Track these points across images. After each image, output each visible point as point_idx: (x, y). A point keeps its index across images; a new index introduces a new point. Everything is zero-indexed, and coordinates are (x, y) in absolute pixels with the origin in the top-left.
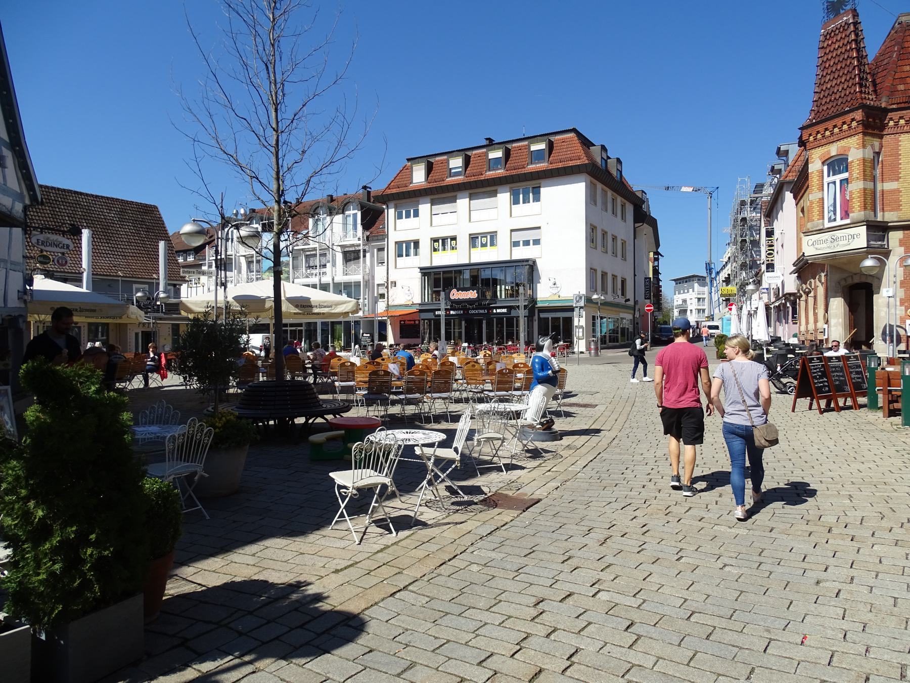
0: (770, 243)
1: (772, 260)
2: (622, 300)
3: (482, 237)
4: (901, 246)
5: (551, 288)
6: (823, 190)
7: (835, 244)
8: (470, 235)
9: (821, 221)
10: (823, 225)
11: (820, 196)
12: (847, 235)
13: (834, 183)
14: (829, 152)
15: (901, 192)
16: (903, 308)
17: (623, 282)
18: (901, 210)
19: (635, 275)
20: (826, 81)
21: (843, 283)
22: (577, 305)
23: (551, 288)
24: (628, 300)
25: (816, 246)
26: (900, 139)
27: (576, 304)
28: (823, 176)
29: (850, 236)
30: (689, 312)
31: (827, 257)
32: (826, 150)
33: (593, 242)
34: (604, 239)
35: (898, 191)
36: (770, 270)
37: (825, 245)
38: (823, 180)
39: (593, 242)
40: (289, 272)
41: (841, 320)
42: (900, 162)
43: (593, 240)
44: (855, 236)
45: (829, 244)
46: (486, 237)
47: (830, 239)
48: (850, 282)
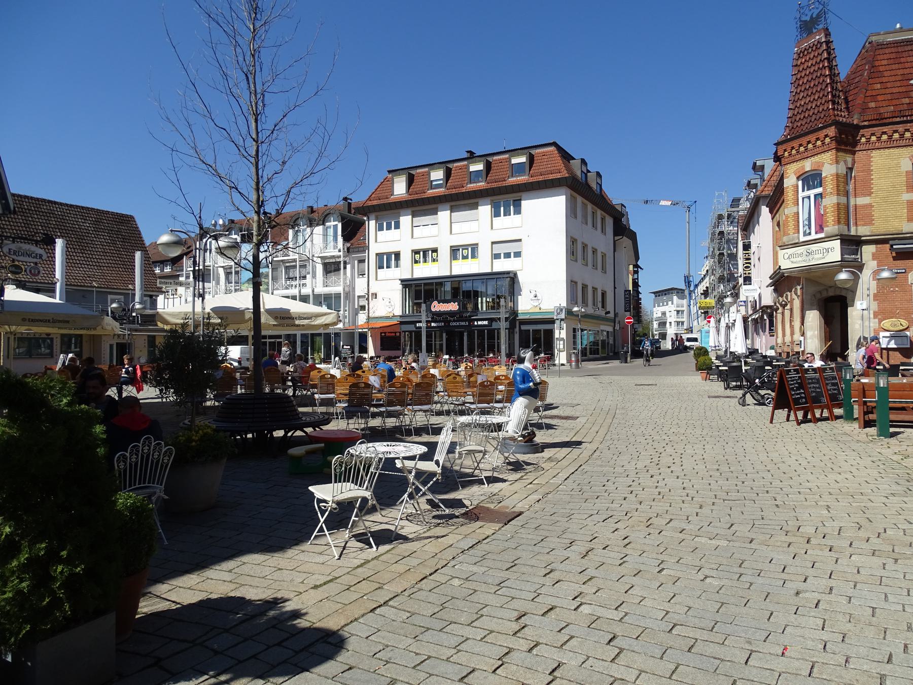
0: (747, 257)
1: (749, 273)
2: (602, 313)
3: (463, 249)
4: (873, 259)
5: (532, 300)
6: (798, 204)
7: (811, 257)
8: (451, 247)
9: (796, 235)
10: (799, 239)
11: (795, 210)
12: (821, 249)
13: (809, 197)
14: (803, 167)
15: (873, 206)
16: (877, 320)
17: (604, 294)
18: (874, 224)
19: (615, 288)
20: (800, 98)
21: (818, 296)
22: (558, 318)
23: (532, 300)
24: (608, 313)
25: (792, 259)
26: (872, 155)
27: (556, 316)
28: (798, 191)
29: (825, 250)
30: (668, 325)
31: (802, 270)
32: (800, 165)
33: (573, 255)
34: (584, 251)
35: (870, 206)
36: (747, 283)
37: (800, 259)
38: (798, 195)
39: (573, 255)
40: (268, 283)
41: (816, 332)
42: (872, 177)
43: (573, 252)
44: (830, 250)
45: (804, 258)
46: (467, 249)
47: (805, 253)
48: (825, 295)
